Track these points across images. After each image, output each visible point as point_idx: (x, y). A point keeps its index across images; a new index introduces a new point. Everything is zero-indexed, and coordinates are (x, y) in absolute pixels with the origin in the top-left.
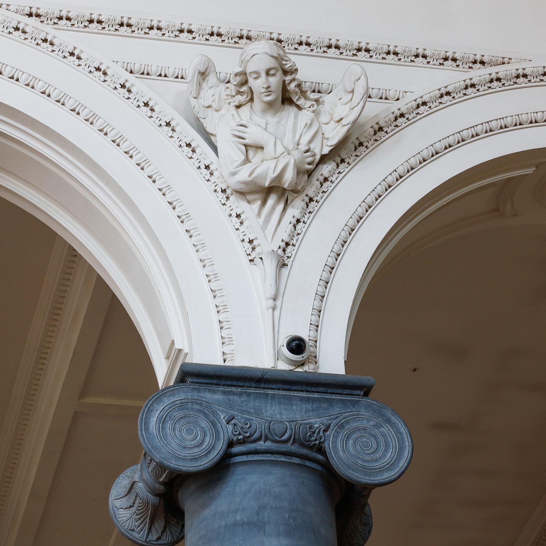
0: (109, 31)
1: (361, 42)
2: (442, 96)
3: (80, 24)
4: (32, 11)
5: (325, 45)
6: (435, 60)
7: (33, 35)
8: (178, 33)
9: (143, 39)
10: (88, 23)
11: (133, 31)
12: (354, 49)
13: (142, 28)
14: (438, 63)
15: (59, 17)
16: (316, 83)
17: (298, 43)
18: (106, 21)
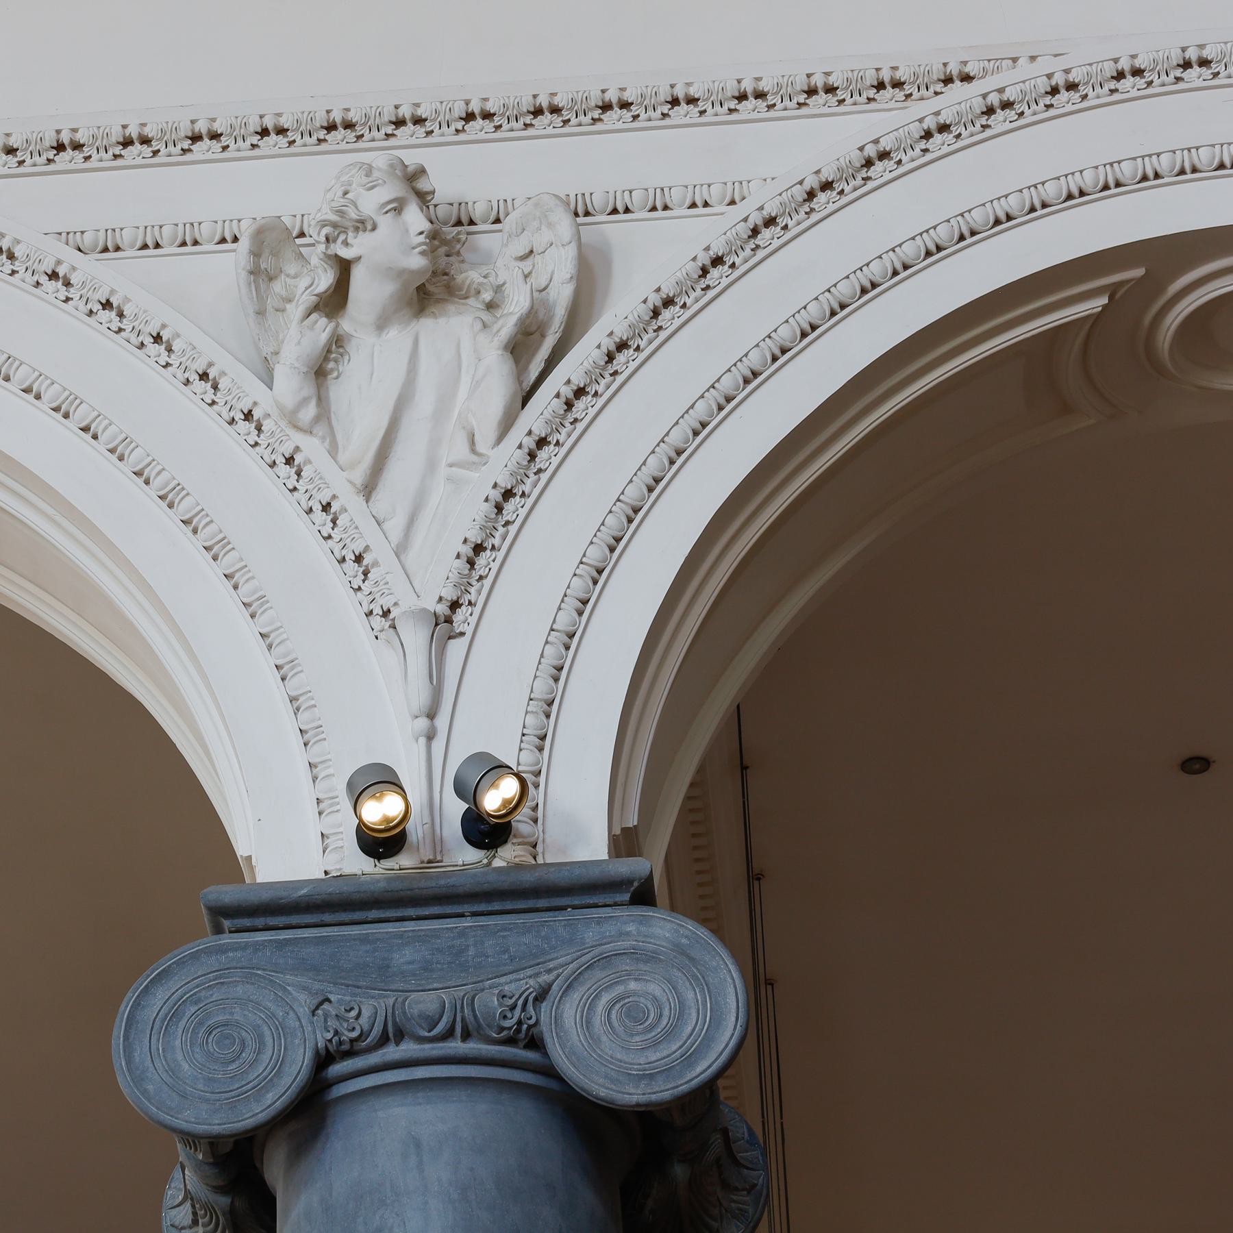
1: (814, 74)
3: (718, 108)
4: (881, 78)
6: (170, 145)
9: (783, 120)
10: (806, 96)
11: (87, 158)
12: (183, 138)
13: (106, 147)
14: (588, 119)
15: (737, 94)
17: (734, 97)
18: (704, 96)
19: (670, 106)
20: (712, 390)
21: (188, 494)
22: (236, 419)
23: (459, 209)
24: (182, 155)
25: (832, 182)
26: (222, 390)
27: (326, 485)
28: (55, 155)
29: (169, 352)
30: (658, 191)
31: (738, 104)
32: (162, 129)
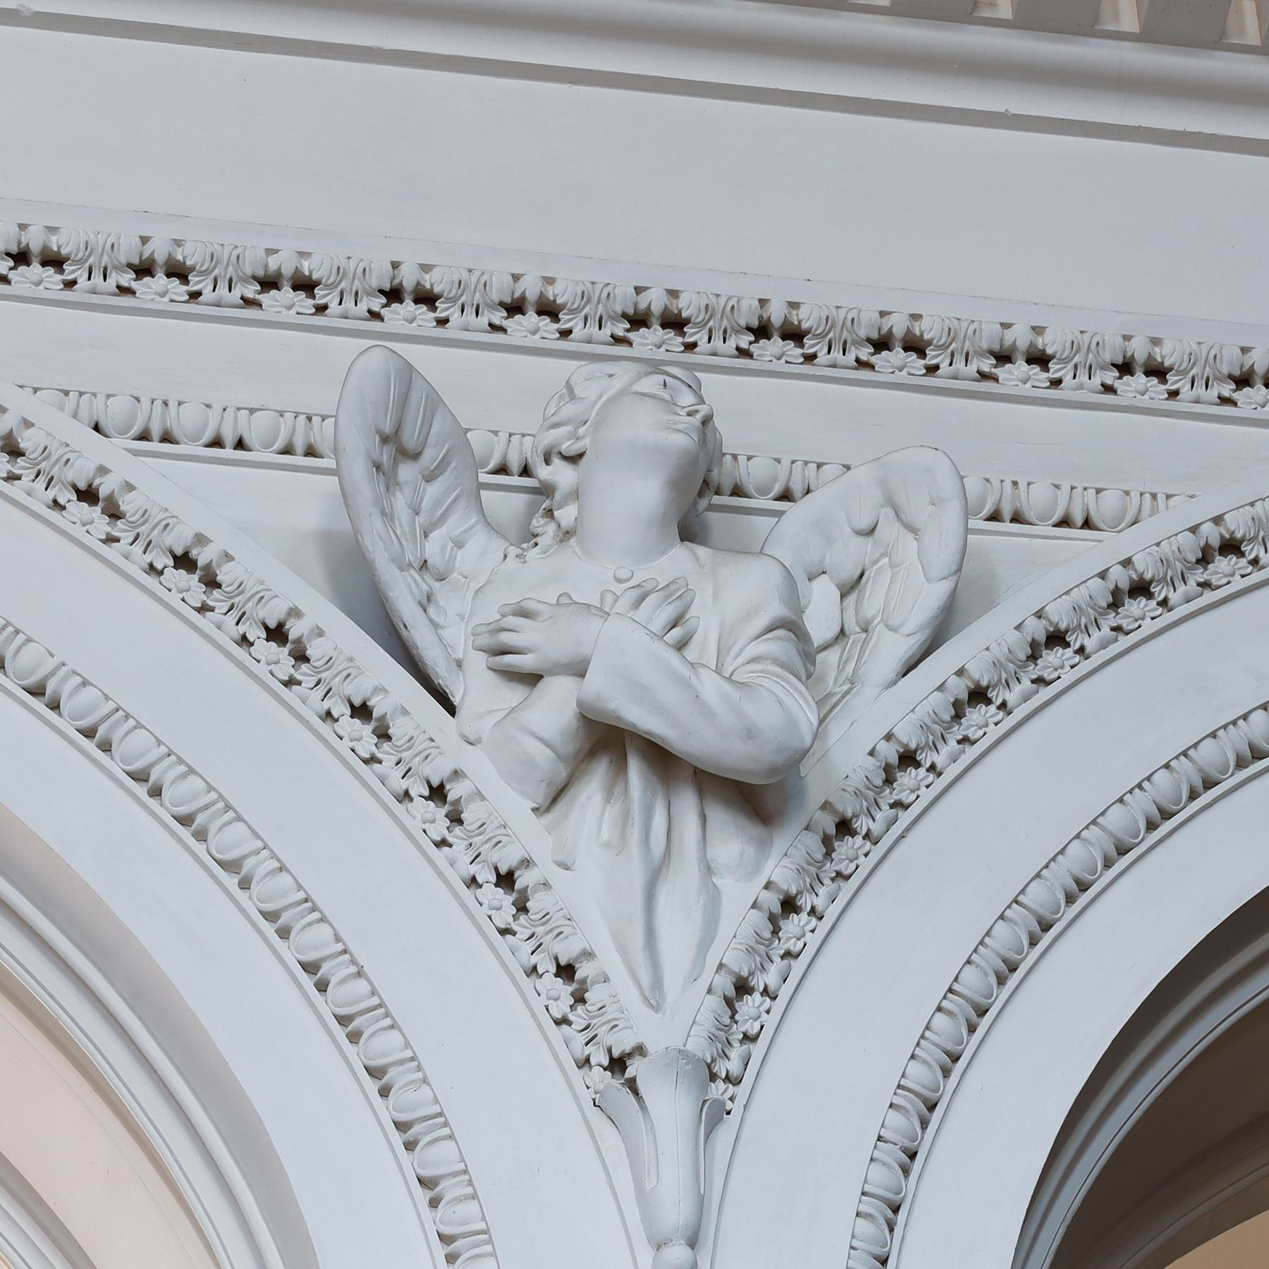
0: (1197, 401)
1: (650, 288)
2: (1205, 559)
5: (743, 323)
8: (869, 353)
12: (985, 351)
19: (12, 264)
20: (1182, 758)
23: (78, 405)
24: (1218, 405)
27: (438, 751)
28: (11, 269)
30: (158, 404)
31: (874, 354)
32: (950, 329)
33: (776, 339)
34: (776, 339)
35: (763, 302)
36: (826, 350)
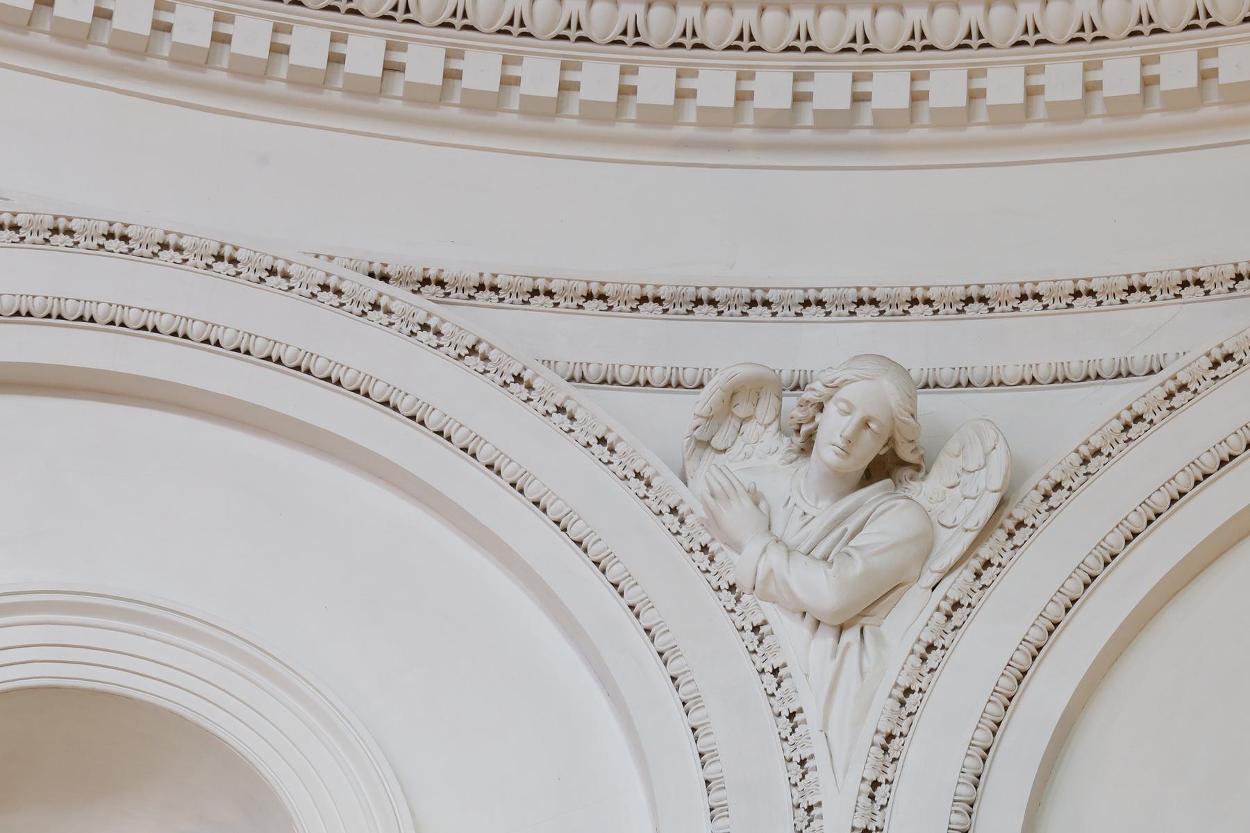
7: (498, 366)
16: (21, 296)
21: (618, 562)
22: (722, 588)
25: (20, 227)
26: (618, 453)
29: (711, 561)
33: (117, 240)
34: (117, 240)
35: (425, 269)
36: (673, 307)
